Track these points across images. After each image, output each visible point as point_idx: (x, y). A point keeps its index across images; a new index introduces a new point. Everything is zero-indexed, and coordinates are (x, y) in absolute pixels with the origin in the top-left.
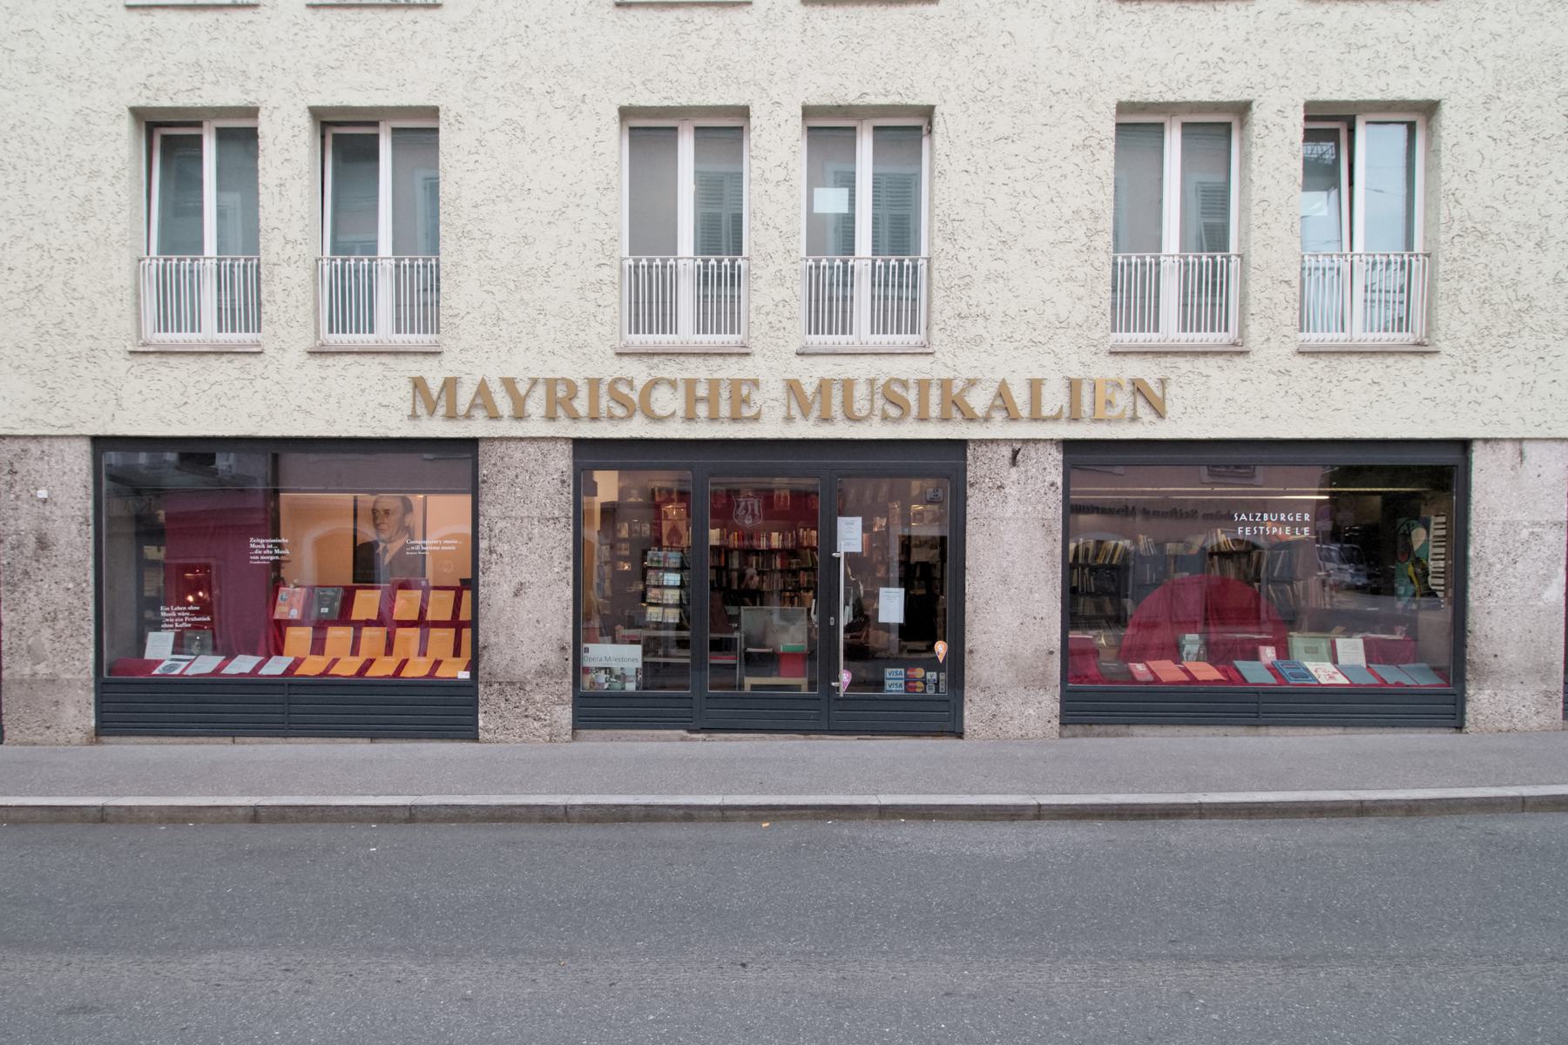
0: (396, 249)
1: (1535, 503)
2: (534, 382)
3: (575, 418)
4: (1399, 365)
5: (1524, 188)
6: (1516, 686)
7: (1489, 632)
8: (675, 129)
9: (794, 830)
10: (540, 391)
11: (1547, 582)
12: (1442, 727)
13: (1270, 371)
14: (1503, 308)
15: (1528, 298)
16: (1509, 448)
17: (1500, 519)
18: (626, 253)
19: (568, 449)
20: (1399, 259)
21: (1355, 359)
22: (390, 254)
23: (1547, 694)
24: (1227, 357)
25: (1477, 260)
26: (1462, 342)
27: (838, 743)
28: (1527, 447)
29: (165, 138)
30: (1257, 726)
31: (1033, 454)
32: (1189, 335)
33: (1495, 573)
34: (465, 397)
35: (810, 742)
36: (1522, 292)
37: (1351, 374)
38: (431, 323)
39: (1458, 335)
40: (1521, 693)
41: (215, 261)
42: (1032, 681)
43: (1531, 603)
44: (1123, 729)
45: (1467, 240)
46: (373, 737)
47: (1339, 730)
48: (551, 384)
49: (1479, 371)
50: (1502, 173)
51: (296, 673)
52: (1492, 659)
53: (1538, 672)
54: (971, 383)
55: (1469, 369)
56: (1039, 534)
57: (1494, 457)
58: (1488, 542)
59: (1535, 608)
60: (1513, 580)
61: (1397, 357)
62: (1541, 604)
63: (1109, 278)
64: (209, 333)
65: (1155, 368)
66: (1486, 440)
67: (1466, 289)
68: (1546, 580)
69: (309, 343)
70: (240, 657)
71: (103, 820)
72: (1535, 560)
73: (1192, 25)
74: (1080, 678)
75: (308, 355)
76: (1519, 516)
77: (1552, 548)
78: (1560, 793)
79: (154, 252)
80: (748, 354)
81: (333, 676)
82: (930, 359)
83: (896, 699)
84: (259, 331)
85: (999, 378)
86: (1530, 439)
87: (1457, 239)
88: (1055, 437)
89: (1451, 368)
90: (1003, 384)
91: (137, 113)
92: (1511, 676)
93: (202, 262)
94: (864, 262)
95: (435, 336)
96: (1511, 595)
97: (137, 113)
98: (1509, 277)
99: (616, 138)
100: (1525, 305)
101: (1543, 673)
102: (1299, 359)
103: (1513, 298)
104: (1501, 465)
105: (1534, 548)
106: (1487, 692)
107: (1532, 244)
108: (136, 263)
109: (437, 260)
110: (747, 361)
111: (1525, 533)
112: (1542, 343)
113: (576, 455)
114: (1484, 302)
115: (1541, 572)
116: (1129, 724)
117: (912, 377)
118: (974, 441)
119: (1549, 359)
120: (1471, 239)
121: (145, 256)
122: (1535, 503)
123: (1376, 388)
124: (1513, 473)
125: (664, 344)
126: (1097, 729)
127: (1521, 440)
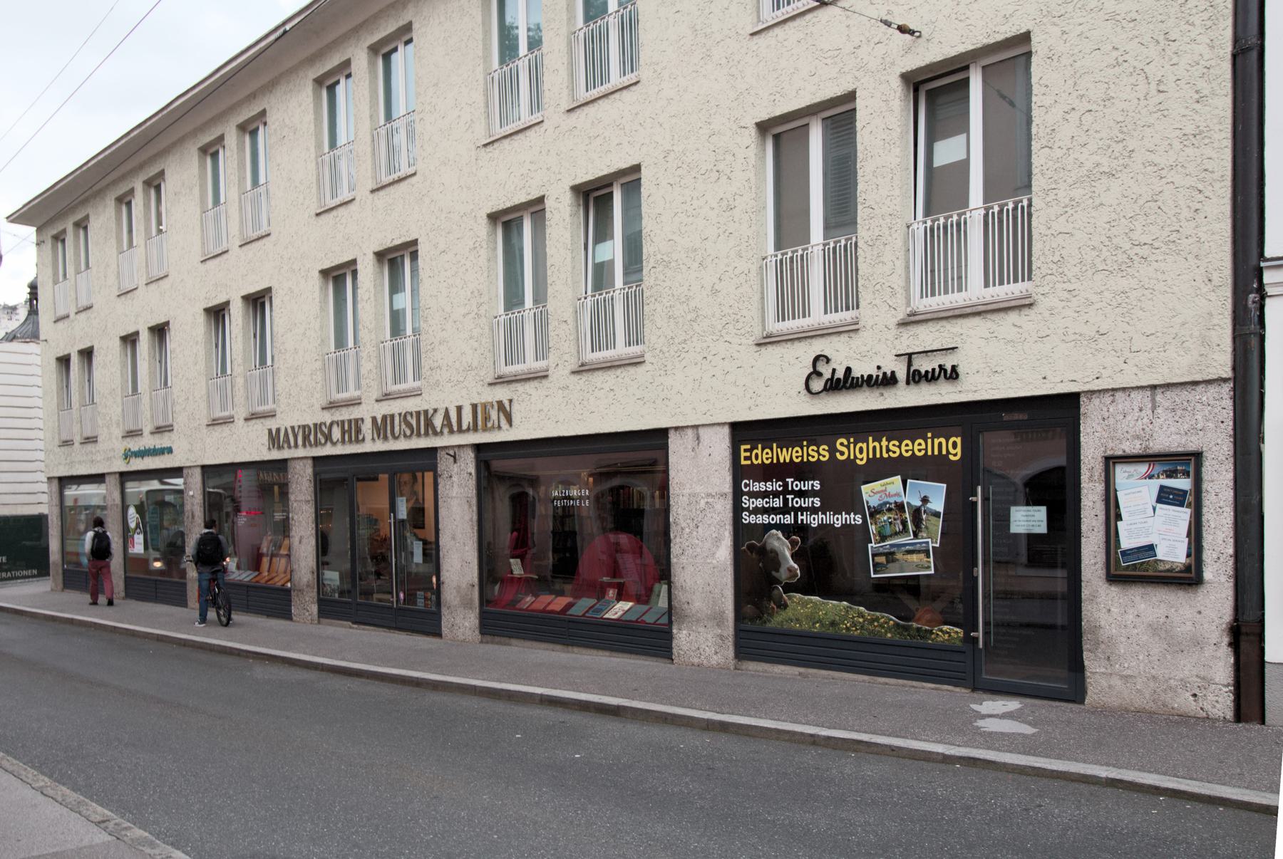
0: (987, 198)
1: (708, 477)
2: (299, 427)
3: (334, 444)
4: (624, 374)
5: (691, 219)
6: (701, 629)
7: (684, 584)
8: (808, 124)
9: (386, 690)
10: (301, 431)
11: (718, 544)
12: (548, 642)
13: (559, 388)
14: (681, 320)
15: (696, 309)
16: (690, 432)
17: (686, 491)
18: (388, 336)
19: (310, 462)
20: (774, 259)
21: (600, 373)
22: (980, 204)
23: (721, 637)
24: (539, 380)
25: (665, 284)
26: (657, 351)
27: (419, 638)
28: (701, 431)
29: (596, 199)
30: (568, 645)
31: (462, 455)
32: (991, 290)
33: (686, 536)
34: (438, 421)
35: (392, 635)
36: (692, 304)
37: (599, 385)
38: (852, 302)
39: (656, 346)
40: (705, 635)
41: (821, 247)
42: (467, 604)
43: (709, 561)
44: (506, 640)
45: (658, 270)
46: (268, 616)
47: (607, 653)
48: (304, 427)
49: (668, 373)
50: (676, 211)
51: (568, 613)
52: (686, 606)
53: (715, 619)
54: (435, 411)
55: (662, 373)
56: (466, 507)
57: (681, 442)
58: (680, 511)
59: (711, 565)
60: (697, 541)
61: (622, 369)
62: (714, 562)
63: (859, 260)
64: (976, 291)
65: (508, 392)
66: (676, 428)
67: (659, 309)
68: (717, 541)
69: (758, 334)
70: (584, 599)
71: (184, 645)
72: (709, 525)
73: (516, 151)
74: (489, 602)
75: (757, 348)
76: (698, 489)
77: (721, 515)
78: (567, 696)
79: (589, 292)
80: (1030, 305)
81: (571, 615)
82: (420, 398)
83: (420, 611)
84: (1030, 279)
85: (444, 406)
86: (703, 425)
87: (653, 270)
88: (468, 443)
89: (652, 373)
90: (447, 409)
91: (167, 323)
92: (698, 621)
93: (810, 250)
94: (979, 211)
95: (1027, 284)
96: (695, 554)
97: (167, 323)
98: (683, 295)
99: (752, 153)
100: (693, 315)
101: (718, 619)
102: (576, 378)
103: (687, 311)
104: (686, 448)
105: (709, 515)
106: (684, 632)
107: (696, 265)
108: (906, 229)
109: (1030, 201)
110: (857, 341)
111: (703, 503)
112: (705, 345)
113: (314, 466)
114: (670, 317)
115: (714, 535)
116: (510, 637)
117: (414, 409)
118: (1084, 392)
119: (709, 358)
120: (660, 268)
121: (913, 221)
122: (708, 477)
123: (612, 393)
124: (693, 454)
125: (935, 307)
126: (497, 639)
127: (696, 427)
